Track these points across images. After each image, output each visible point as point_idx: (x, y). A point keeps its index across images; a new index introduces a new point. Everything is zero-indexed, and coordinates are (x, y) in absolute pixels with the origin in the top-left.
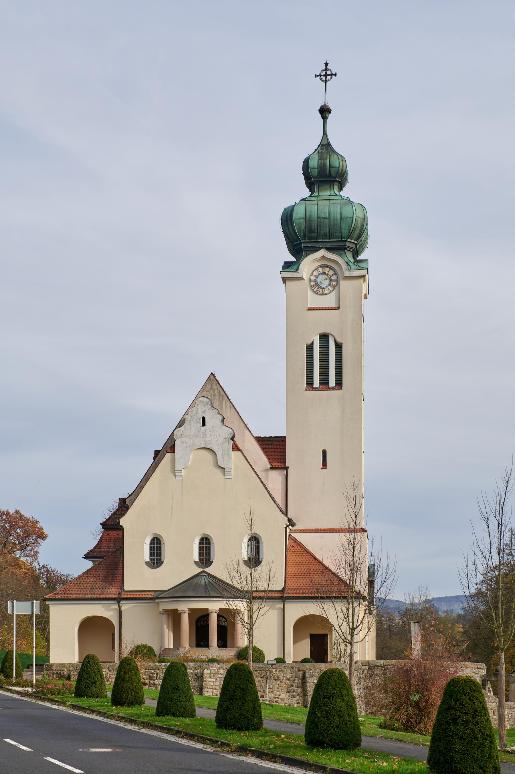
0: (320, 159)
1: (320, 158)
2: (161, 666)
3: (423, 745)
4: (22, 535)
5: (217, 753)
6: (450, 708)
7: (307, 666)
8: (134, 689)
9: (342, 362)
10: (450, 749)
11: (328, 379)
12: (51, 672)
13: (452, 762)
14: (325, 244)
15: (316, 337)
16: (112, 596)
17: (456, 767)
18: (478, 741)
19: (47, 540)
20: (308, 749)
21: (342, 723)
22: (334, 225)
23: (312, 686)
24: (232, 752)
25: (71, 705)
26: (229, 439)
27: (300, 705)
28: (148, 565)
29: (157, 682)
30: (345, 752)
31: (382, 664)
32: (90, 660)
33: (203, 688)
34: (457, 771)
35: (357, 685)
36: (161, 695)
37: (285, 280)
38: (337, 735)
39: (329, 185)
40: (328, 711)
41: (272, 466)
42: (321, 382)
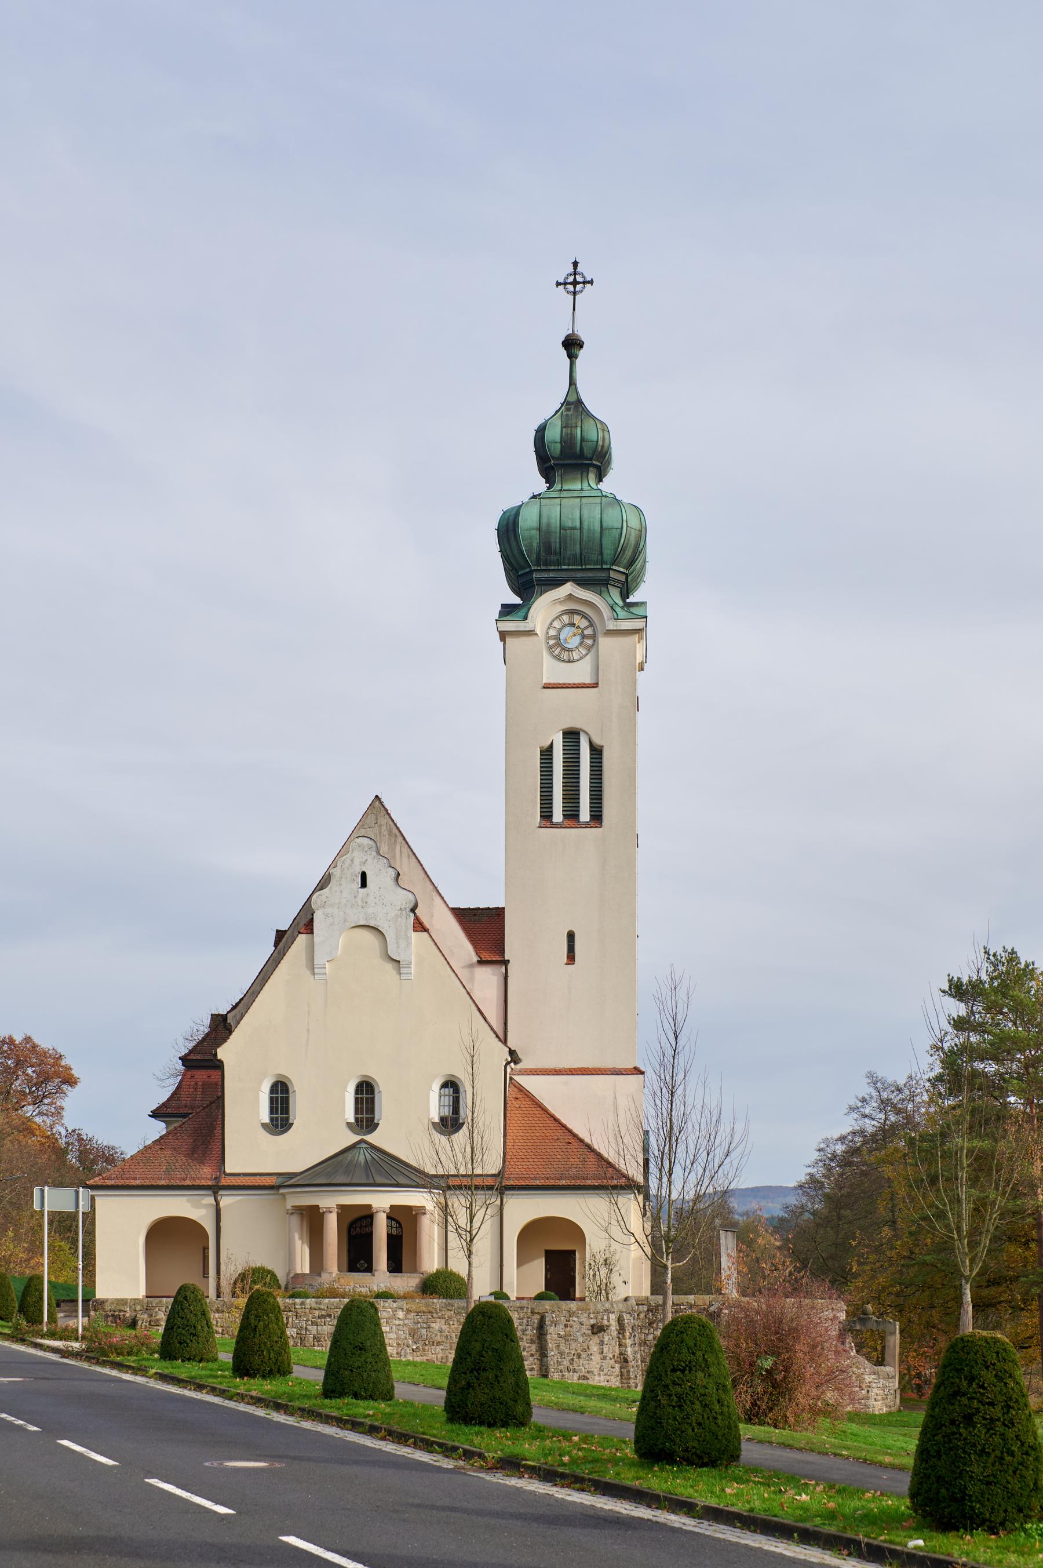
1: (564, 425)
2: (295, 1304)
3: (836, 1455)
4: (36, 1078)
5: (463, 1471)
6: (957, 1393)
7: (547, 1305)
8: (275, 1348)
9: (601, 779)
10: (961, 1473)
11: (577, 809)
13: (963, 1499)
14: (573, 574)
15: (558, 734)
16: (203, 1182)
17: (972, 1508)
18: (1014, 1457)
19: (78, 1087)
20: (641, 1465)
21: (708, 1418)
24: (489, 1468)
25: (156, 1373)
26: (408, 910)
27: (535, 1373)
30: (715, 1472)
32: (188, 1294)
34: (975, 1517)
35: (630, 1338)
36: (332, 1360)
37: (503, 635)
38: (698, 1441)
40: (681, 1395)
41: (481, 958)
42: (565, 813)
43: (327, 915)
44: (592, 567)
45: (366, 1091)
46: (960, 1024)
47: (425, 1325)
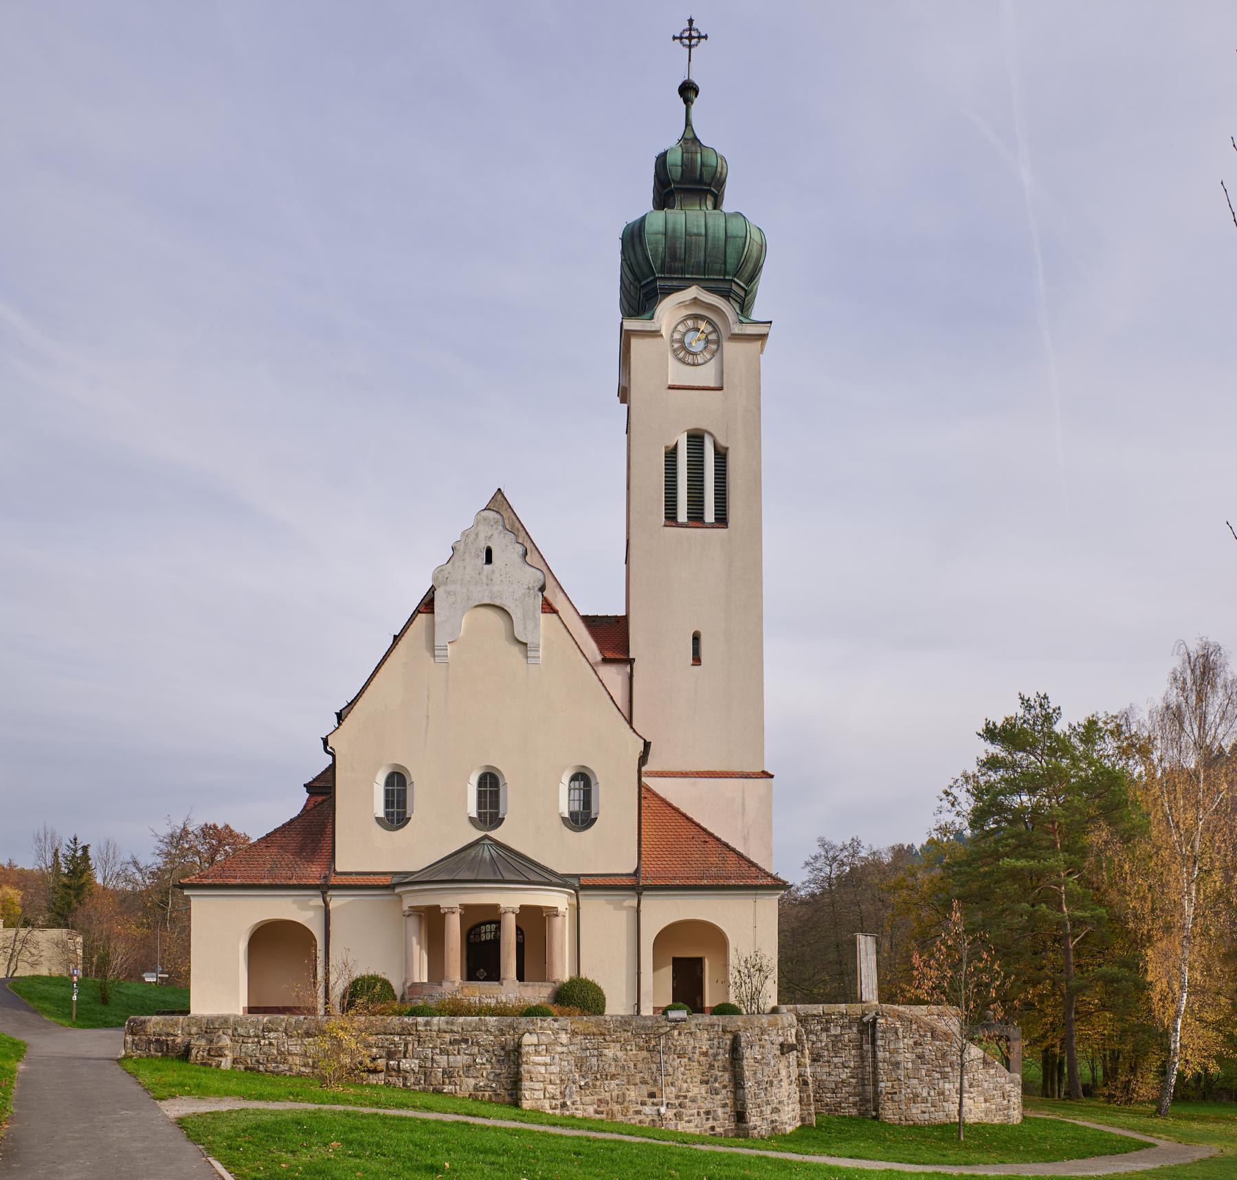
0: (686, 152)
12: (143, 1037)
15: (682, 436)
16: (311, 882)
22: (714, 248)
23: (752, 1066)
26: (537, 589)
28: (382, 824)
29: (407, 1065)
31: (821, 1012)
33: (520, 1080)
39: (698, 199)
42: (690, 515)
43: (449, 593)
44: (715, 277)
45: (490, 784)
46: (992, 763)
47: (596, 1053)
